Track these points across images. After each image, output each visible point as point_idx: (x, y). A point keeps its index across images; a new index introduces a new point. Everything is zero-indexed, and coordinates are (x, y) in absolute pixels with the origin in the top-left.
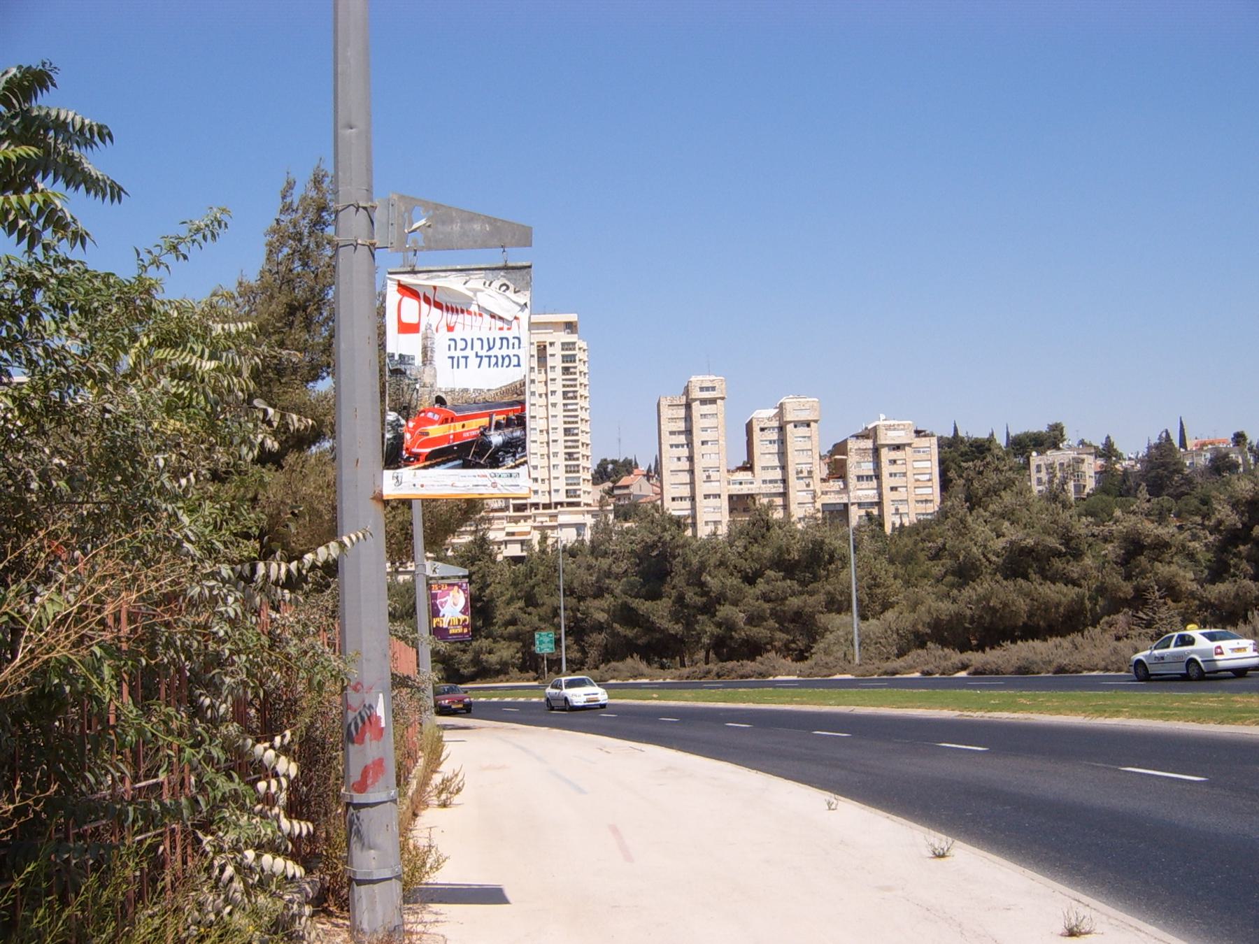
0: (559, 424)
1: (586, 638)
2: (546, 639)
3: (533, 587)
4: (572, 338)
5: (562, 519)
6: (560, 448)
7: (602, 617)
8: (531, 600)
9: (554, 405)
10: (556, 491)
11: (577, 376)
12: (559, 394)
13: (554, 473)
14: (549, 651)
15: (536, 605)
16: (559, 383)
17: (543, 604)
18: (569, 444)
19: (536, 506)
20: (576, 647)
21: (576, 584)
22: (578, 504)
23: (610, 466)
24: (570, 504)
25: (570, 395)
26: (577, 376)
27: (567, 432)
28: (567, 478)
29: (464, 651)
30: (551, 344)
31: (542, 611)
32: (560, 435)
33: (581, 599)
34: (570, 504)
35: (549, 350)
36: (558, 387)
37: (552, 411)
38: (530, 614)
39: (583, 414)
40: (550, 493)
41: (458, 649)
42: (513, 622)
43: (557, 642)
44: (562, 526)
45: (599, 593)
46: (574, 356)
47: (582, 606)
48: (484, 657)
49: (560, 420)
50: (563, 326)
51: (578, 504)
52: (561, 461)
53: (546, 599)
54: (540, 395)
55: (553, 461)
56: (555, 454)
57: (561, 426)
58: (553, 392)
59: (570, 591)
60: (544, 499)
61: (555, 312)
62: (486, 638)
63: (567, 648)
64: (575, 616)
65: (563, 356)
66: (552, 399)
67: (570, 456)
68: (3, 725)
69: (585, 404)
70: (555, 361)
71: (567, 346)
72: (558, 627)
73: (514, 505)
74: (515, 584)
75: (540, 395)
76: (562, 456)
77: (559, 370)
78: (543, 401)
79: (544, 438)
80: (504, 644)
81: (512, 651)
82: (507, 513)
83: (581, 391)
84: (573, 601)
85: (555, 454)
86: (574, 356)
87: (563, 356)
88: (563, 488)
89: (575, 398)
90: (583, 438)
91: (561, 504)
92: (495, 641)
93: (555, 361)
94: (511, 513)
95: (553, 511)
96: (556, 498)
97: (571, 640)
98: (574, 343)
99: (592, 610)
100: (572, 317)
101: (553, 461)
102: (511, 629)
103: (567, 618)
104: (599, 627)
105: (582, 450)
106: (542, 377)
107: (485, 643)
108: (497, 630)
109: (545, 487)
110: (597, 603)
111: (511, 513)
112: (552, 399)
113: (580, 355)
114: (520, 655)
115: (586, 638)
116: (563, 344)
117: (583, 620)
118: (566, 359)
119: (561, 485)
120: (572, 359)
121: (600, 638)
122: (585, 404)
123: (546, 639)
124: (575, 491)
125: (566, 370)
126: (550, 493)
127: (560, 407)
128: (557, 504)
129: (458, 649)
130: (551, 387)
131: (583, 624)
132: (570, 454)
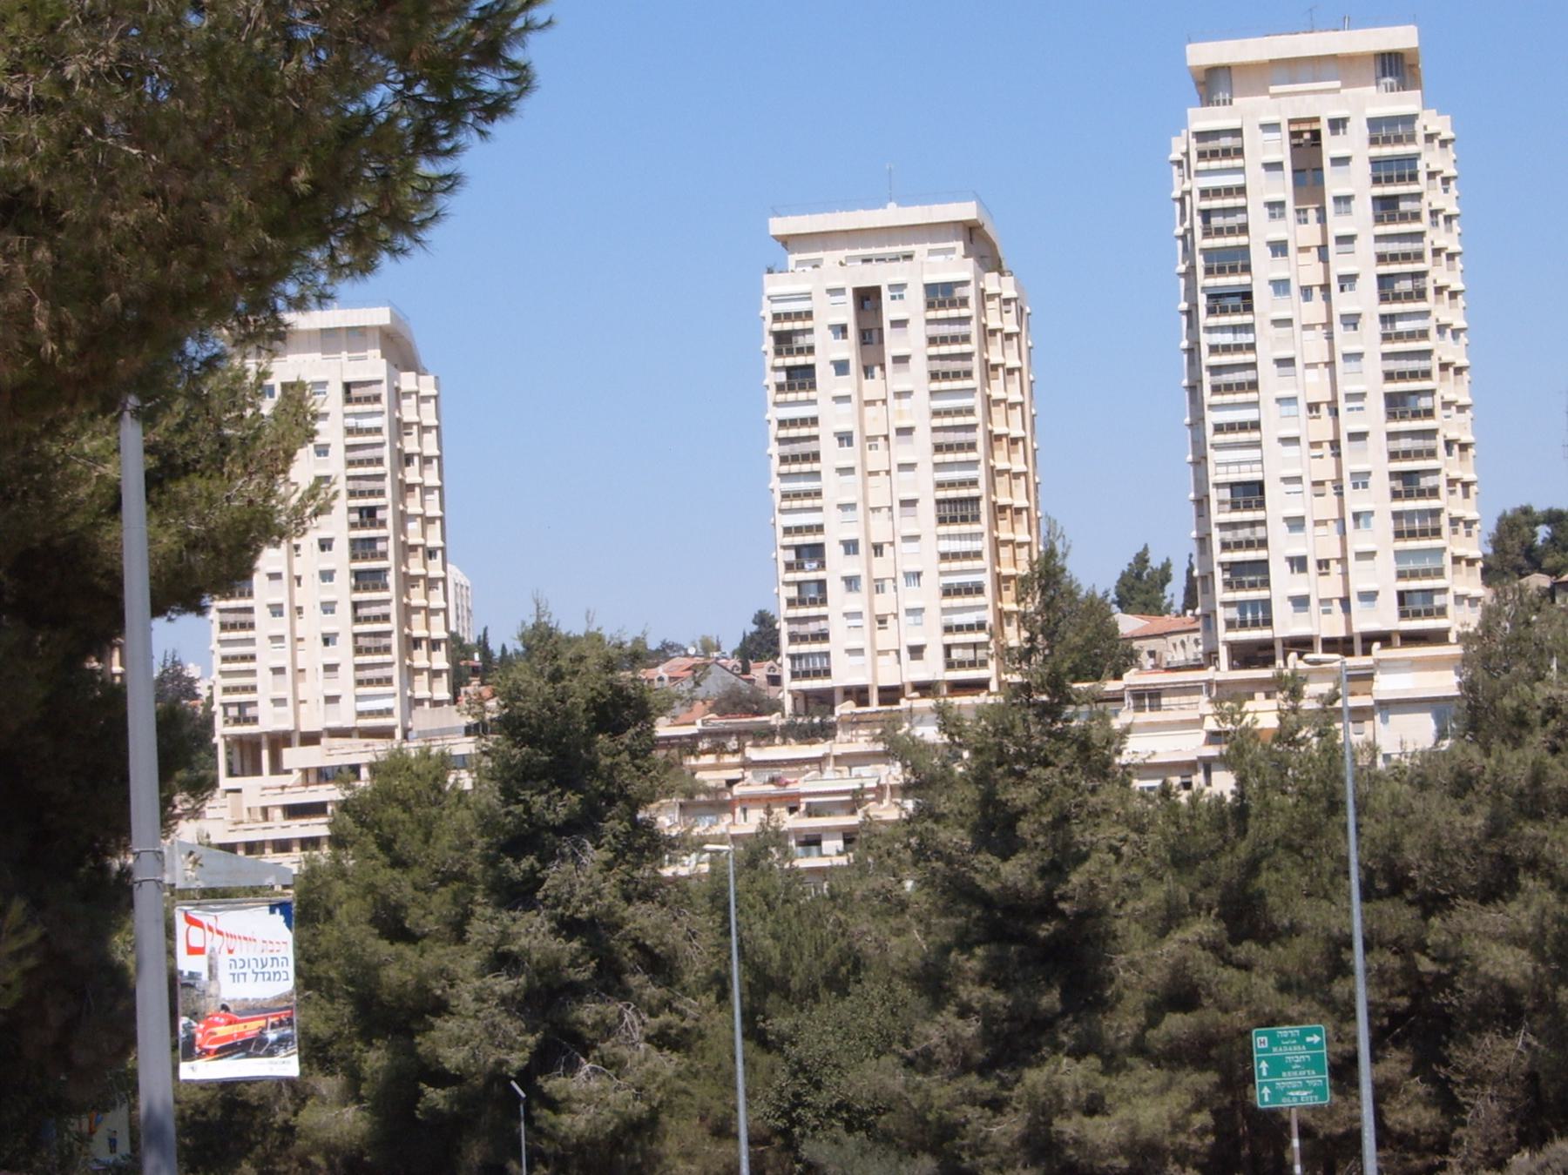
0: (1370, 379)
1: (1455, 1052)
2: (1296, 1054)
3: (1252, 867)
4: (1404, 103)
5: (1388, 685)
6: (1374, 459)
7: (1510, 965)
8: (1244, 917)
9: (1352, 321)
10: (1369, 596)
11: (1423, 225)
12: (1368, 286)
13: (1359, 540)
14: (1306, 1098)
15: (1268, 935)
16: (1366, 248)
17: (1294, 930)
18: (1405, 444)
19: (1302, 645)
20: (1418, 1087)
21: (1411, 853)
22: (1439, 637)
23: (1543, 532)
24: (1411, 638)
25: (1405, 286)
26: (1423, 225)
27: (1396, 405)
28: (1400, 555)
29: (996, 1105)
30: (1337, 125)
31: (1288, 955)
32: (1373, 417)
33: (1432, 904)
34: (1411, 638)
35: (1332, 146)
36: (1363, 261)
37: (1346, 341)
38: (1246, 967)
39: (1447, 350)
40: (1345, 602)
41: (973, 1099)
42: (1182, 994)
43: (1343, 1072)
44: (1388, 707)
45: (1498, 885)
46: (1413, 159)
47: (1438, 930)
48: (1068, 1126)
49: (1374, 367)
50: (1372, 69)
51: (1439, 637)
52: (1378, 499)
53: (1307, 912)
54: (1306, 292)
55: (1356, 501)
56: (1361, 480)
57: (1377, 388)
58: (1348, 280)
59: (1387, 881)
60: (1334, 626)
61: (1344, 22)
62: (1078, 1053)
63: (1382, 1091)
64: (1410, 971)
65: (1375, 162)
66: (1343, 303)
67: (1407, 483)
68: (1431, 1171)
69: (1452, 314)
70: (1351, 180)
71: (1382, 129)
72: (1348, 1014)
73: (1233, 647)
74: (1181, 860)
75: (1306, 292)
76: (1381, 485)
77: (1363, 208)
78: (1314, 310)
79: (1322, 428)
80: (1145, 1074)
81: (1177, 1101)
82: (1209, 674)
83: (1440, 274)
84: (1400, 917)
85: (1361, 480)
86: (1413, 159)
87: (1375, 162)
88: (1389, 586)
89: (1421, 295)
90: (1452, 426)
91: (1385, 639)
92: (1112, 1065)
93: (1351, 180)
94: (1223, 671)
95: (1358, 661)
96: (1366, 620)
97: (1397, 1062)
98: (1410, 119)
99: (1473, 945)
100: (1401, 37)
101: (1356, 501)
102: (1176, 1024)
103: (1379, 977)
104: (1505, 1009)
105: (1451, 466)
106: (1310, 233)
107: (1069, 1074)
108: (1122, 1025)
109: (1331, 586)
110: (1493, 918)
111: (1223, 671)
112: (1343, 303)
113: (1432, 159)
114: (1203, 1119)
115: (1455, 1052)
116: (1374, 123)
117: (1442, 982)
118: (1384, 170)
119: (1381, 576)
120: (1403, 169)
121: (1504, 1052)
122: (1452, 314)
123: (1296, 1054)
124: (1429, 593)
125: (1386, 207)
126: (1345, 602)
127: (1371, 327)
128: (1368, 639)
129: (973, 1099)
130: (1340, 265)
131: (1440, 999)
132: (1408, 477)
